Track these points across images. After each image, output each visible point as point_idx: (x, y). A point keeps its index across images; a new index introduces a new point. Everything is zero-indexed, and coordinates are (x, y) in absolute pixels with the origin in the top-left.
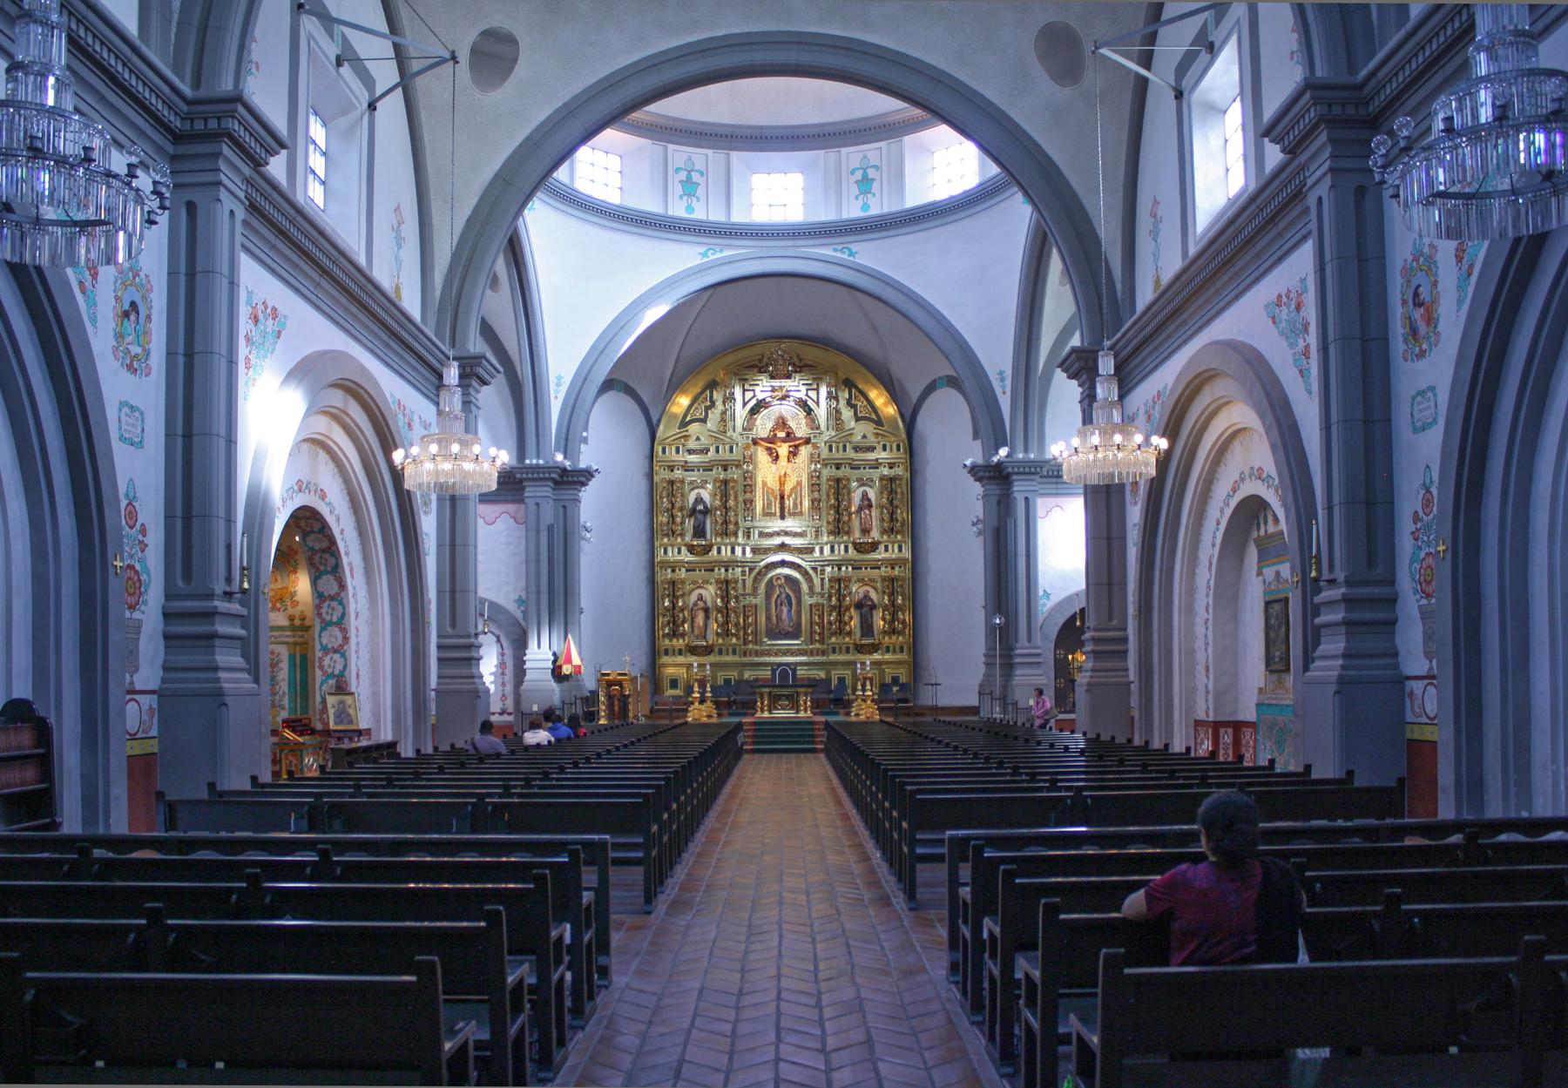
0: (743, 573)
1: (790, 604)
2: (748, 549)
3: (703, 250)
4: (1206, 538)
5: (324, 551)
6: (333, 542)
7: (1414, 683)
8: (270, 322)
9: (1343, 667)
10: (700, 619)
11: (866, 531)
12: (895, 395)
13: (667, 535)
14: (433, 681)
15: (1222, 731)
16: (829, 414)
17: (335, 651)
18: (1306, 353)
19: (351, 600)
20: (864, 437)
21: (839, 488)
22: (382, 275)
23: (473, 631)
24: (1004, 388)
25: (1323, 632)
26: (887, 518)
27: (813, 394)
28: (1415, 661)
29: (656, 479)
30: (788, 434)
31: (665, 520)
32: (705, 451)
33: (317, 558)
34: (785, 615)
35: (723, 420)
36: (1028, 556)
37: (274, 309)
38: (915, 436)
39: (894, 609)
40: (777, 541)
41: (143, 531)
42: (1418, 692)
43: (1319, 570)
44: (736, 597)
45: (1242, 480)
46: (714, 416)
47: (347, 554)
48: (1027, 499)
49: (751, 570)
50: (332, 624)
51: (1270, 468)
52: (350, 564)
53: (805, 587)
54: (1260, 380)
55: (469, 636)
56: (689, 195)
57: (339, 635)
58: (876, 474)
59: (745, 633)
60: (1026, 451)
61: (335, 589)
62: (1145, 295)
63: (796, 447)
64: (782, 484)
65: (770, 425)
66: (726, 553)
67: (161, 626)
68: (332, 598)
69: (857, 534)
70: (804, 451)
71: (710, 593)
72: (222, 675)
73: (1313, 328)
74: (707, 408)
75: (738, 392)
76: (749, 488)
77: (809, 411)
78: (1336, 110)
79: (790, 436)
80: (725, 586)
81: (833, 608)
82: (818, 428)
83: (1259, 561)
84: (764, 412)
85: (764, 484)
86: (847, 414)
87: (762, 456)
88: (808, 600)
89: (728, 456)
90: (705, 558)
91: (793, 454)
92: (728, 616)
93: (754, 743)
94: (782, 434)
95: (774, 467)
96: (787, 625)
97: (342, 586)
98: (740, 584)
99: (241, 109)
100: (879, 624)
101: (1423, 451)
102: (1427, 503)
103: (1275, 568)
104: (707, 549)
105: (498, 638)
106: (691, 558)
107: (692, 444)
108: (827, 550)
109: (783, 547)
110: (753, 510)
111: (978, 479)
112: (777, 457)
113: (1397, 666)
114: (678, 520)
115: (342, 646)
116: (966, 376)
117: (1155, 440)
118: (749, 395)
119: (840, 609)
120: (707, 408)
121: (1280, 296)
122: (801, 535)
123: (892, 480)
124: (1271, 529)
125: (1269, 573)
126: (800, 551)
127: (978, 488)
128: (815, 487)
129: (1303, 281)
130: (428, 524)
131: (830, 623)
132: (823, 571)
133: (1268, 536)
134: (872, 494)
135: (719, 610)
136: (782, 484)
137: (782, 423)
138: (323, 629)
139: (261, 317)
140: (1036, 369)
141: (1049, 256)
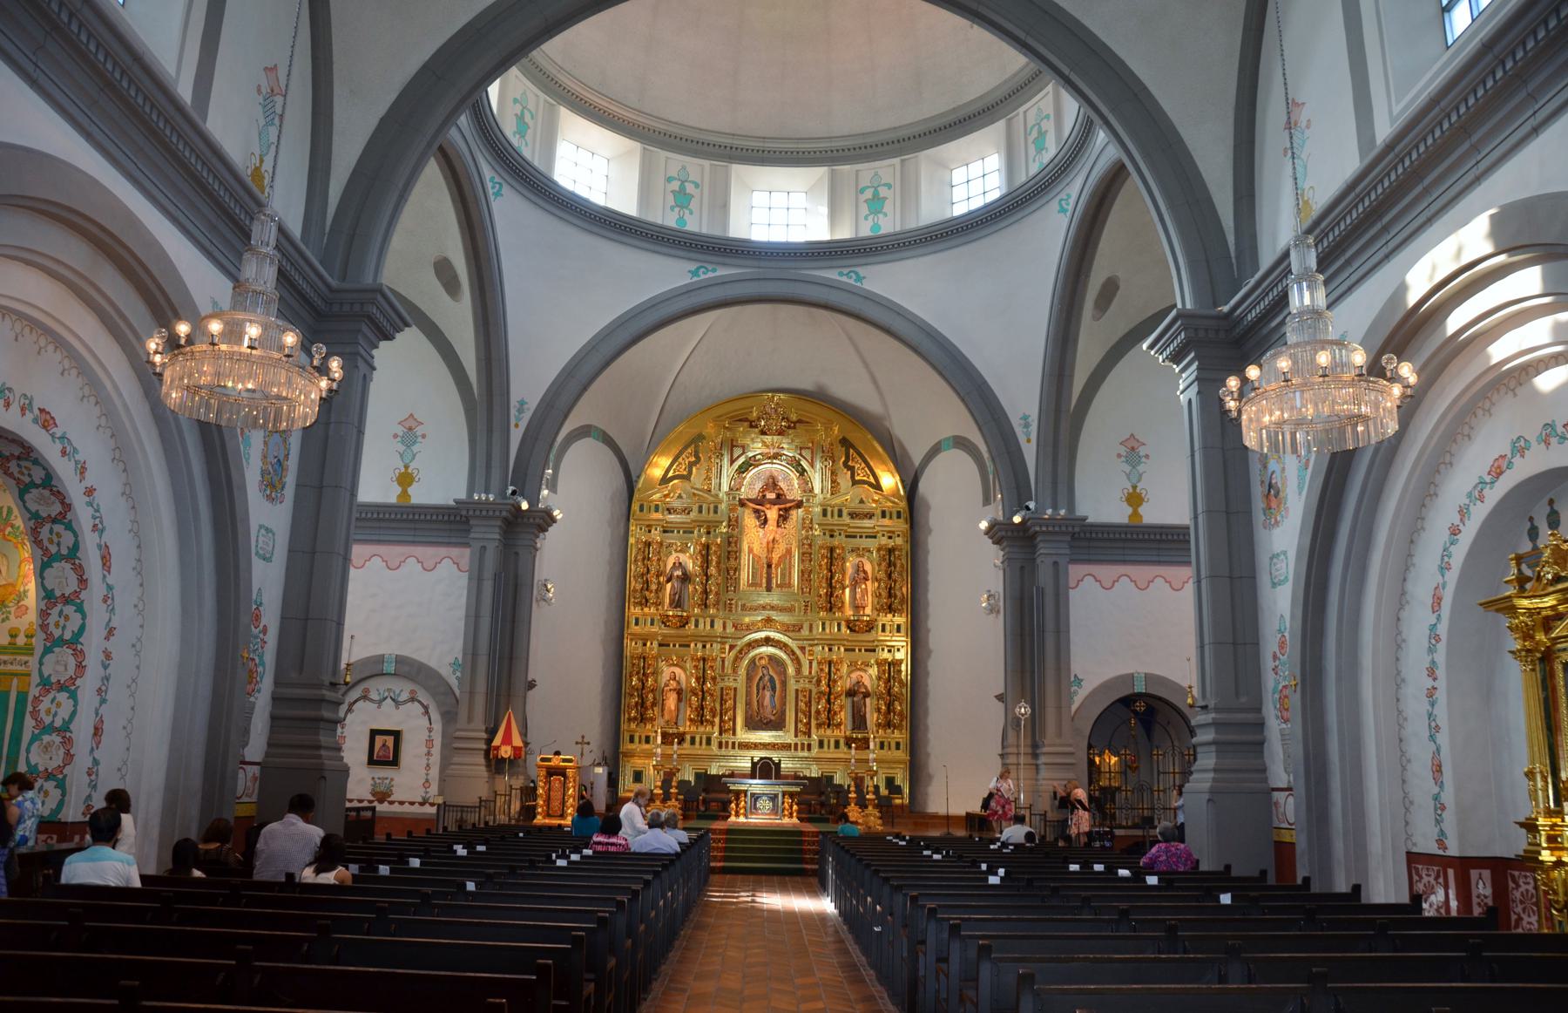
0: (722, 650)
1: (774, 689)
3: (693, 266)
7: (1275, 794)
9: (1214, 780)
11: (857, 607)
12: (899, 461)
13: (640, 604)
14: (256, 748)
15: (1474, 873)
17: (61, 687)
21: (833, 557)
24: (1028, 435)
25: (1199, 749)
26: (885, 594)
28: (1279, 775)
29: (632, 540)
30: (779, 496)
31: (639, 587)
33: (44, 532)
34: (767, 701)
36: (1058, 631)
38: (917, 502)
39: (890, 698)
41: (265, 631)
42: (1282, 801)
44: (714, 679)
49: (732, 647)
50: (62, 642)
53: (791, 670)
55: (320, 686)
56: (682, 207)
57: (72, 662)
58: (872, 544)
59: (721, 720)
60: (1055, 508)
61: (72, 585)
63: (787, 510)
64: (770, 550)
65: (759, 486)
66: (704, 626)
67: (269, 709)
68: (66, 600)
69: (849, 612)
70: (797, 515)
71: (685, 676)
72: (323, 752)
74: (691, 465)
78: (1201, 334)
85: (751, 550)
87: (749, 520)
88: (792, 686)
90: (681, 632)
91: (783, 517)
92: (703, 699)
93: (725, 859)
96: (768, 713)
98: (718, 663)
99: (379, 298)
100: (872, 718)
101: (1280, 603)
102: (1282, 645)
104: (684, 622)
105: (426, 708)
109: (768, 621)
110: (737, 580)
112: (766, 521)
113: (1265, 780)
114: (654, 587)
115: (73, 680)
119: (829, 697)
120: (691, 465)
122: (790, 610)
123: (891, 551)
127: (993, 555)
128: (806, 556)
131: (818, 712)
134: (868, 567)
136: (770, 550)
137: (772, 483)
138: (47, 651)
140: (755, 889)
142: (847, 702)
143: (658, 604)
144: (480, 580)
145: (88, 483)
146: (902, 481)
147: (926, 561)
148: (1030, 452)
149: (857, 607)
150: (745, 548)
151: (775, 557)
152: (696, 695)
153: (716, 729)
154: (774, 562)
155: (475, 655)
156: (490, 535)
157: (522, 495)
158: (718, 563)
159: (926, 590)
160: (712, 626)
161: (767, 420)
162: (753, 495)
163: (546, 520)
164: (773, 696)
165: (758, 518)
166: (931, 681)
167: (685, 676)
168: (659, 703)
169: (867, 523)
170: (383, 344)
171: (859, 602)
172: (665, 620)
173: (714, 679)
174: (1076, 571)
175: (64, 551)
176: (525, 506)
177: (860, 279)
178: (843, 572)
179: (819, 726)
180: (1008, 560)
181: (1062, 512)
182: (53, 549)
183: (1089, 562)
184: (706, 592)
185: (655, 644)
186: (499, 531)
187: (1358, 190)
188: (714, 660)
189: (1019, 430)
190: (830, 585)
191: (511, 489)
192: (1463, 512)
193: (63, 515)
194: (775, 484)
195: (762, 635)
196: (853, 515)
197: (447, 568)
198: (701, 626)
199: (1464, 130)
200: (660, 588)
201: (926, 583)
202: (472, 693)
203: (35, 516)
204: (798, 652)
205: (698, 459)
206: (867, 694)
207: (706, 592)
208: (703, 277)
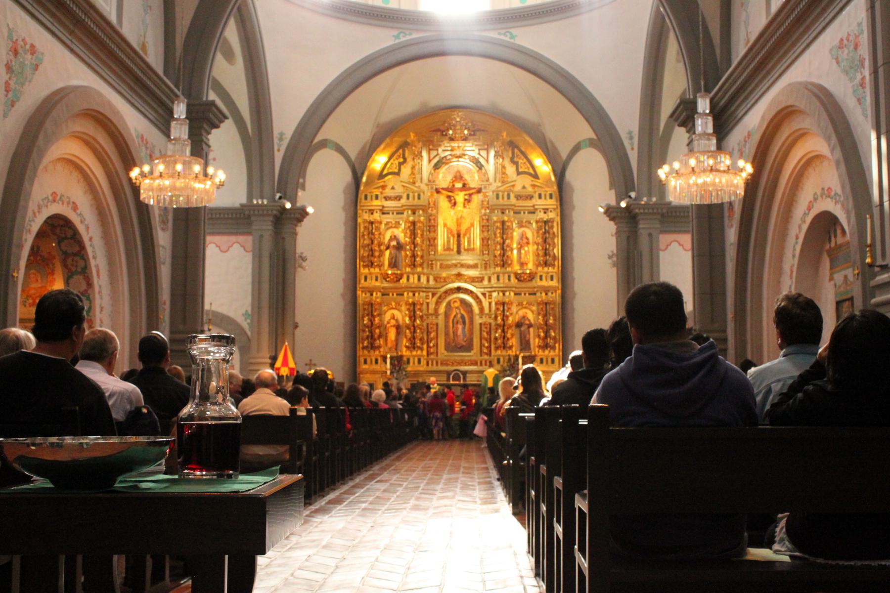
1: (464, 323)
2: (431, 278)
3: (395, 32)
4: (788, 253)
5: (75, 255)
6: (82, 247)
8: (29, 56)
10: (392, 335)
11: (522, 264)
12: (551, 156)
16: (496, 168)
18: (862, 85)
19: (97, 296)
20: (524, 187)
21: (504, 228)
22: (129, 31)
23: (199, 329)
24: (632, 144)
26: (541, 253)
27: (484, 153)
29: (359, 220)
30: (464, 185)
31: (366, 254)
32: (398, 198)
33: (69, 261)
34: (460, 332)
35: (413, 173)
37: (32, 46)
39: (547, 328)
40: (455, 271)
43: (873, 257)
44: (421, 317)
45: (815, 199)
46: (406, 171)
47: (94, 258)
48: (650, 235)
49: (433, 295)
51: (837, 188)
52: (97, 266)
54: (827, 111)
58: (532, 218)
59: (428, 347)
60: (650, 196)
61: (84, 286)
62: (740, 50)
63: (470, 195)
65: (449, 178)
66: (414, 279)
70: (477, 198)
71: (401, 316)
73: (867, 63)
74: (400, 164)
75: (425, 154)
76: (432, 227)
77: (480, 167)
79: (465, 187)
80: (413, 307)
81: (498, 326)
82: (488, 180)
83: (831, 269)
84: (444, 169)
85: (445, 225)
86: (511, 170)
87: (443, 203)
88: (478, 320)
89: (416, 202)
90: (397, 285)
91: (468, 201)
92: (415, 332)
94: (459, 185)
95: (452, 212)
96: (461, 340)
97: (90, 284)
98: (425, 307)
99: (214, 108)
100: (535, 342)
103: (843, 273)
104: (399, 278)
106: (386, 285)
107: (388, 192)
108: (494, 279)
110: (436, 246)
111: (612, 219)
112: (455, 204)
114: (377, 254)
116: (606, 138)
117: (741, 163)
118: (434, 153)
119: (503, 327)
120: (400, 164)
121: (842, 40)
122: (475, 266)
124: (840, 240)
125: (839, 277)
126: (472, 280)
127: (612, 227)
128: (484, 228)
129: (859, 24)
130: (163, 239)
132: (490, 296)
133: (839, 247)
134: (529, 234)
135: (408, 327)
136: (459, 224)
137: (459, 177)
139: (20, 51)
140: (658, 129)
141: (667, 37)
142: (516, 331)
143: (380, 266)
144: (260, 257)
145: (90, 235)
146: (554, 171)
147: (571, 231)
148: (633, 157)
149: (522, 264)
150: (441, 222)
151: (463, 228)
152: (409, 328)
153: (425, 353)
154: (462, 233)
155: (259, 308)
156: (266, 227)
157: (285, 198)
158: (422, 235)
159: (572, 250)
160: (419, 279)
161: (454, 130)
162: (445, 185)
163: (302, 214)
164: (464, 328)
165: (450, 201)
166: (576, 315)
167: (401, 316)
168: (384, 335)
169: (529, 203)
170: (214, 131)
171: (523, 259)
172: (385, 277)
173: (421, 317)
174: (664, 239)
175: (79, 270)
176: (288, 205)
177: (512, 37)
178: (512, 238)
179: (497, 348)
180: (618, 233)
181: (654, 199)
182: (74, 269)
183: (675, 232)
184: (414, 256)
185: (379, 294)
186: (273, 224)
187: (765, 36)
188: (422, 304)
189: (626, 143)
190: (503, 249)
191: (278, 195)
192: (800, 227)
193: (80, 252)
194: (461, 178)
195: (456, 285)
196: (519, 197)
197: (236, 249)
198: (411, 280)
199: (800, 20)
200: (382, 253)
201: (572, 244)
202: (259, 333)
203: (65, 253)
204: (481, 297)
205: (405, 160)
206: (530, 326)
207: (414, 256)
208: (403, 39)
